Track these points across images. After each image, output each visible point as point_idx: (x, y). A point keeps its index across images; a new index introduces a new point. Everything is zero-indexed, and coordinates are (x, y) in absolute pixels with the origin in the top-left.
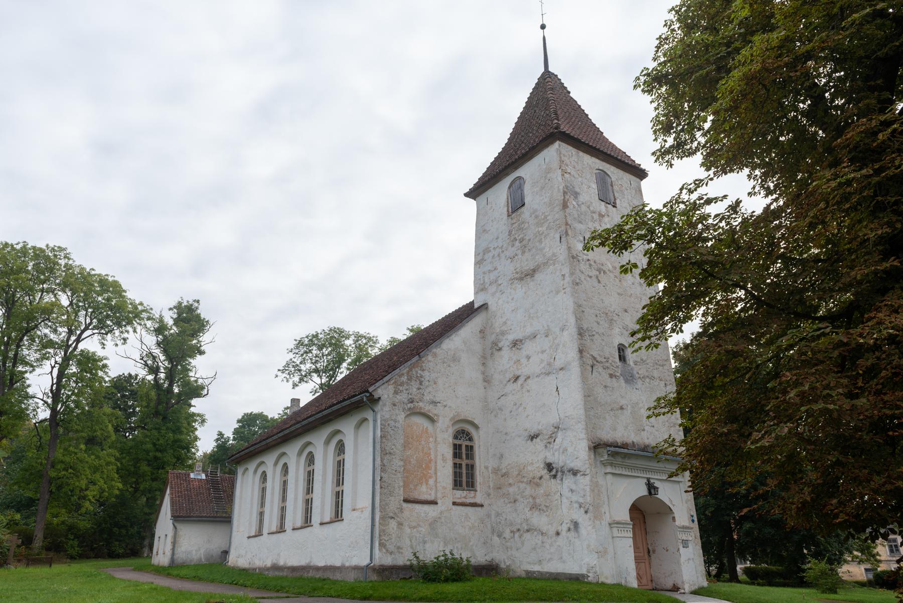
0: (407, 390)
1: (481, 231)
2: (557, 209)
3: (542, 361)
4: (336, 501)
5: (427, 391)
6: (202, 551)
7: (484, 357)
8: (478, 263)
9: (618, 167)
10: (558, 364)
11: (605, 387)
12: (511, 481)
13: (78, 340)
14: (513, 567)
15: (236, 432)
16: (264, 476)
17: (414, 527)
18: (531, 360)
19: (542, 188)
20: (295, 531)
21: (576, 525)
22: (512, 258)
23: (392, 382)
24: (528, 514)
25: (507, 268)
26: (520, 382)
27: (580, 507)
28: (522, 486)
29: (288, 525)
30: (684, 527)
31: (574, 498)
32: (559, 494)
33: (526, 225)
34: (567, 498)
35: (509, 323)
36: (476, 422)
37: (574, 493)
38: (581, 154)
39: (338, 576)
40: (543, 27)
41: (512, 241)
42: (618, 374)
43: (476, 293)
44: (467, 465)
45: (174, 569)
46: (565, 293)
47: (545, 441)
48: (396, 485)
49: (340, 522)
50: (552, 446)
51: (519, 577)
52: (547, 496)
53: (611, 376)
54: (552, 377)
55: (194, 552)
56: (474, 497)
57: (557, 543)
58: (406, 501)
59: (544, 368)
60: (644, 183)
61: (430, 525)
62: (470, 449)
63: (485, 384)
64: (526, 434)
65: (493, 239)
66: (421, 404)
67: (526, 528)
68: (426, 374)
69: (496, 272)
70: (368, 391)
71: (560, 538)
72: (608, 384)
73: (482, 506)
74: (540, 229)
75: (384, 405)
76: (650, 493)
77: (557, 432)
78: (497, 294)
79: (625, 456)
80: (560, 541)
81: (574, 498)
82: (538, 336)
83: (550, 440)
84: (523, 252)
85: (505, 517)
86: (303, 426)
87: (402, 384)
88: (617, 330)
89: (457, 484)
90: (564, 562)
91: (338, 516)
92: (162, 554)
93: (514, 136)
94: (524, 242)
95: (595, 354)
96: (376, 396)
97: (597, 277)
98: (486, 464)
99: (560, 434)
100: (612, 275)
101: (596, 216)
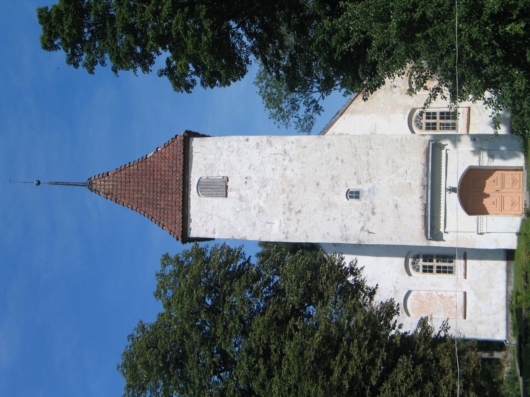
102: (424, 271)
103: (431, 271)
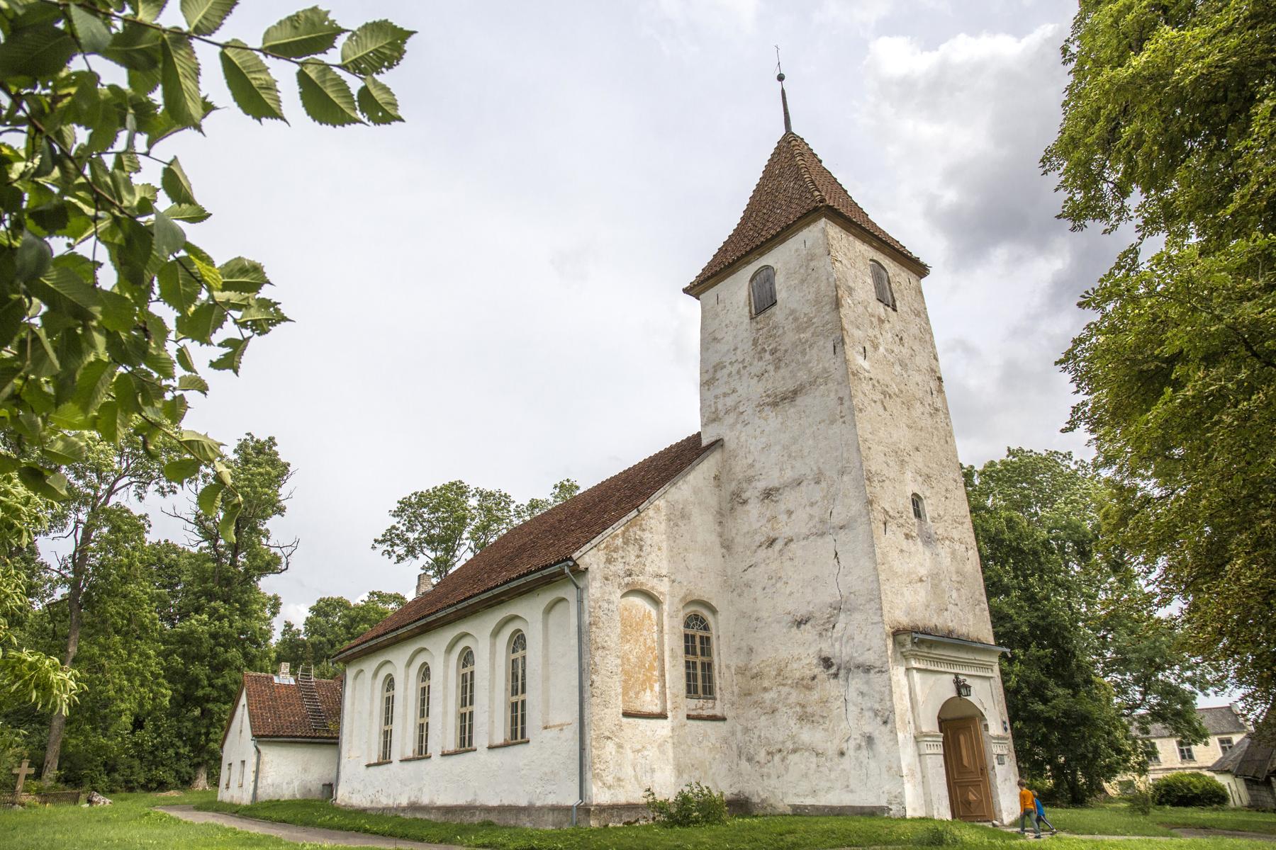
0: (623, 557)
1: (709, 339)
2: (827, 308)
3: (811, 517)
4: (512, 717)
5: (650, 560)
6: (296, 784)
7: (720, 513)
8: (707, 383)
9: (894, 259)
10: (837, 520)
11: (902, 551)
12: (766, 684)
13: (111, 492)
14: (772, 801)
15: (309, 622)
16: (390, 683)
17: (638, 751)
18: (793, 516)
19: (803, 281)
20: (446, 758)
21: (870, 740)
22: (760, 377)
23: (603, 546)
24: (795, 729)
25: (751, 389)
26: (778, 546)
27: (876, 715)
28: (785, 690)
29: (434, 747)
30: (998, 738)
31: (867, 703)
32: (843, 699)
33: (781, 331)
34: (855, 705)
35: (758, 466)
36: (714, 603)
37: (867, 698)
38: (851, 238)
39: (527, 823)
41: (760, 353)
42: (914, 534)
43: (704, 425)
44: (703, 664)
45: (261, 810)
46: (844, 422)
47: (818, 628)
48: (613, 693)
49: (524, 745)
50: (830, 634)
51: (784, 815)
52: (824, 702)
53: (907, 536)
54: (829, 539)
55: (285, 786)
56: (713, 708)
57: (841, 767)
58: (626, 714)
59: (815, 527)
60: (924, 282)
61: (660, 746)
62: (706, 641)
63: (724, 550)
64: (789, 618)
65: (728, 351)
66: (641, 578)
67: (791, 747)
68: (647, 535)
69: (735, 395)
70: (570, 559)
71: (845, 760)
72: (904, 548)
73: (724, 719)
74: (802, 336)
75: (594, 579)
76: (959, 693)
77: (838, 615)
78: (739, 426)
79: (932, 644)
80: (846, 763)
81: (867, 703)
82: (804, 484)
83: (827, 626)
84: (777, 368)
85: (757, 733)
86: (458, 610)
87: (616, 550)
88: (909, 475)
89: (691, 691)
90: (852, 791)
91: (517, 734)
92: (236, 788)
93: (751, 215)
94: (778, 354)
95: (887, 508)
96: (582, 567)
97: (882, 403)
98: (728, 662)
99: (842, 616)
100: (898, 400)
101: (875, 320)
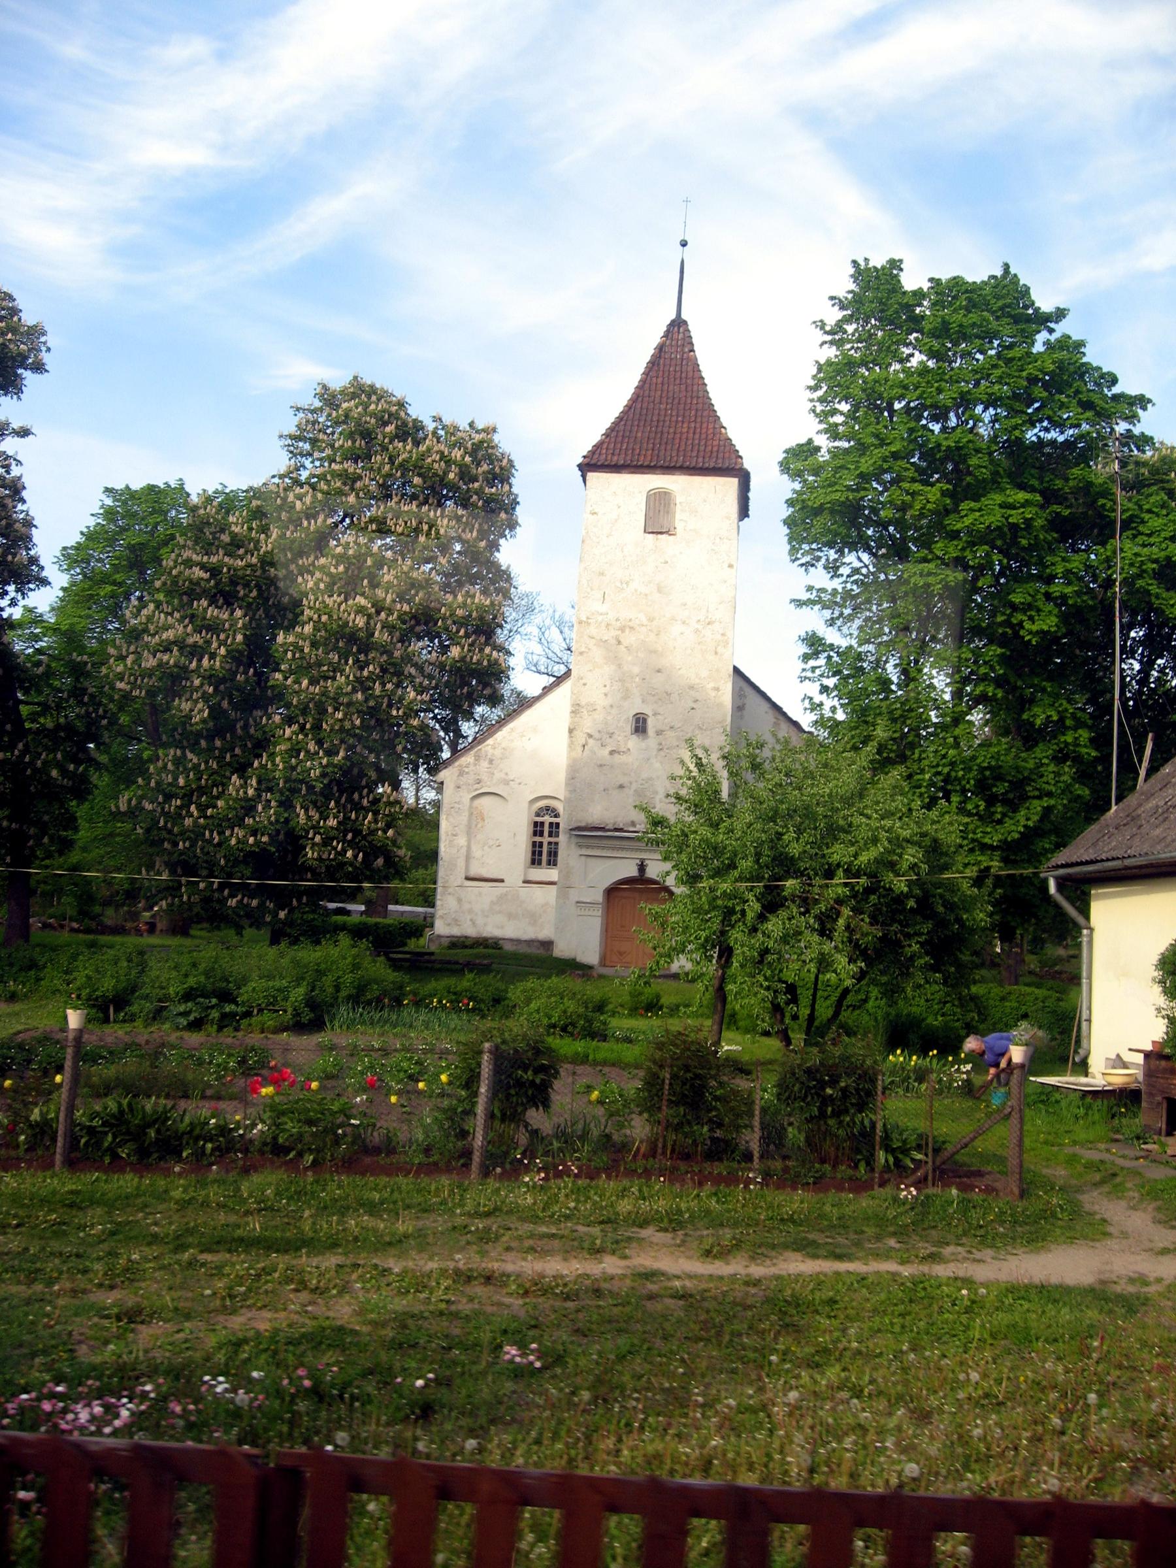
40: (684, 244)
102: (536, 824)
103: (535, 834)
